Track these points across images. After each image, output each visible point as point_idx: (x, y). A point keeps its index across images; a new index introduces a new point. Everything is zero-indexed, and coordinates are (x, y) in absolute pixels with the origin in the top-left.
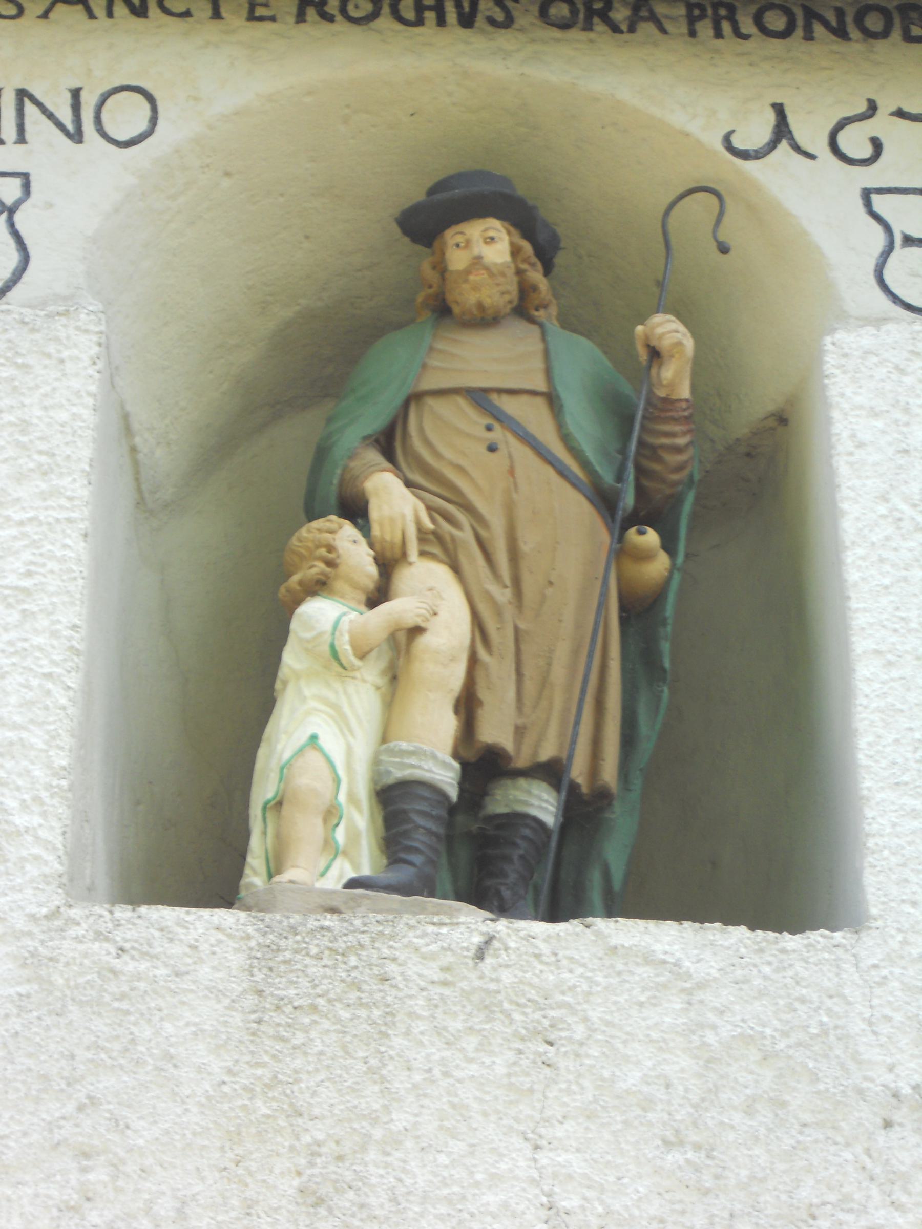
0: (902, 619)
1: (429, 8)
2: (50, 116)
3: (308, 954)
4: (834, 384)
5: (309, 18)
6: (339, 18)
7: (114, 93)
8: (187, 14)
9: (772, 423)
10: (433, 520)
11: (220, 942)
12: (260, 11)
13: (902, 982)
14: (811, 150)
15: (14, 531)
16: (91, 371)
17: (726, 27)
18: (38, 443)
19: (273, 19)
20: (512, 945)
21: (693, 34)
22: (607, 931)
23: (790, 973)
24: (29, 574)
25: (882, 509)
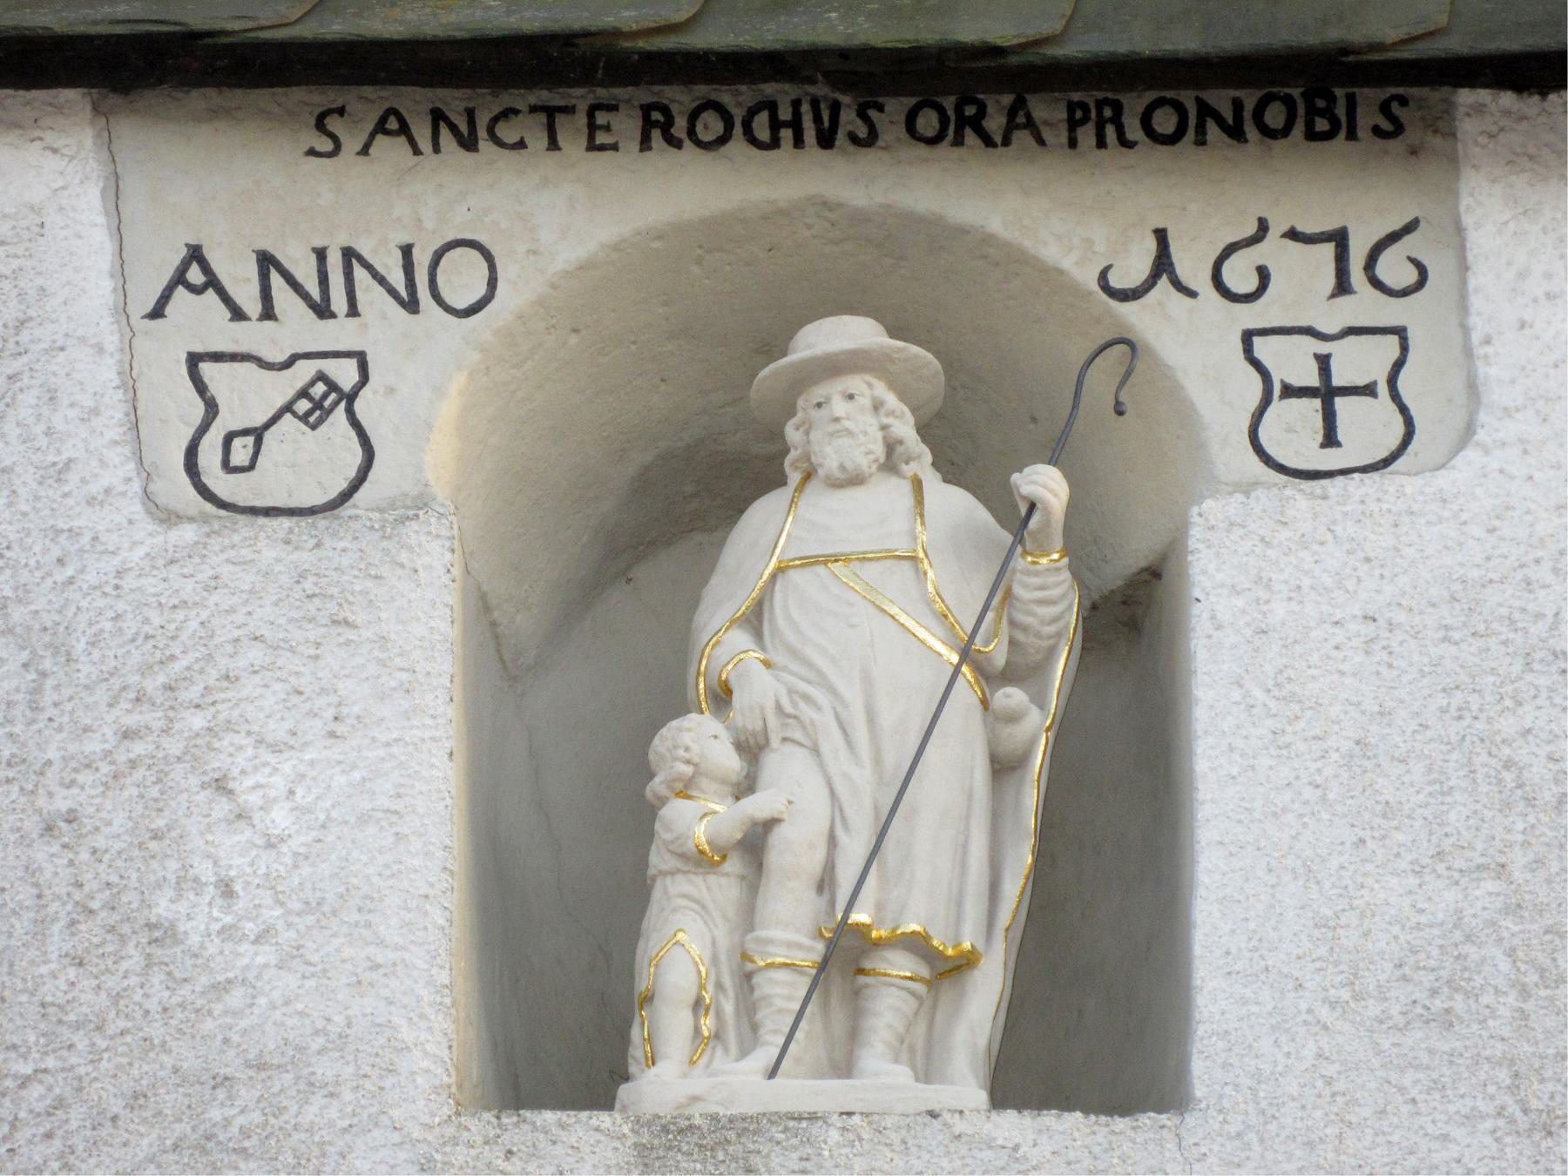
0: (1247, 809)
1: (786, 124)
2: (382, 281)
3: (679, 1150)
4: (1198, 560)
5: (654, 144)
6: (687, 143)
7: (448, 250)
8: (521, 145)
9: (1145, 576)
10: (794, 704)
11: (598, 1142)
12: (601, 138)
13: (1220, 1159)
14: (1192, 285)
15: (381, 752)
16: (445, 579)
17: (1110, 131)
18: (398, 660)
19: (614, 147)
20: (865, 1136)
21: (1073, 143)
22: (951, 1122)
23: (1117, 1153)
24: (399, 796)
25: (1236, 695)
